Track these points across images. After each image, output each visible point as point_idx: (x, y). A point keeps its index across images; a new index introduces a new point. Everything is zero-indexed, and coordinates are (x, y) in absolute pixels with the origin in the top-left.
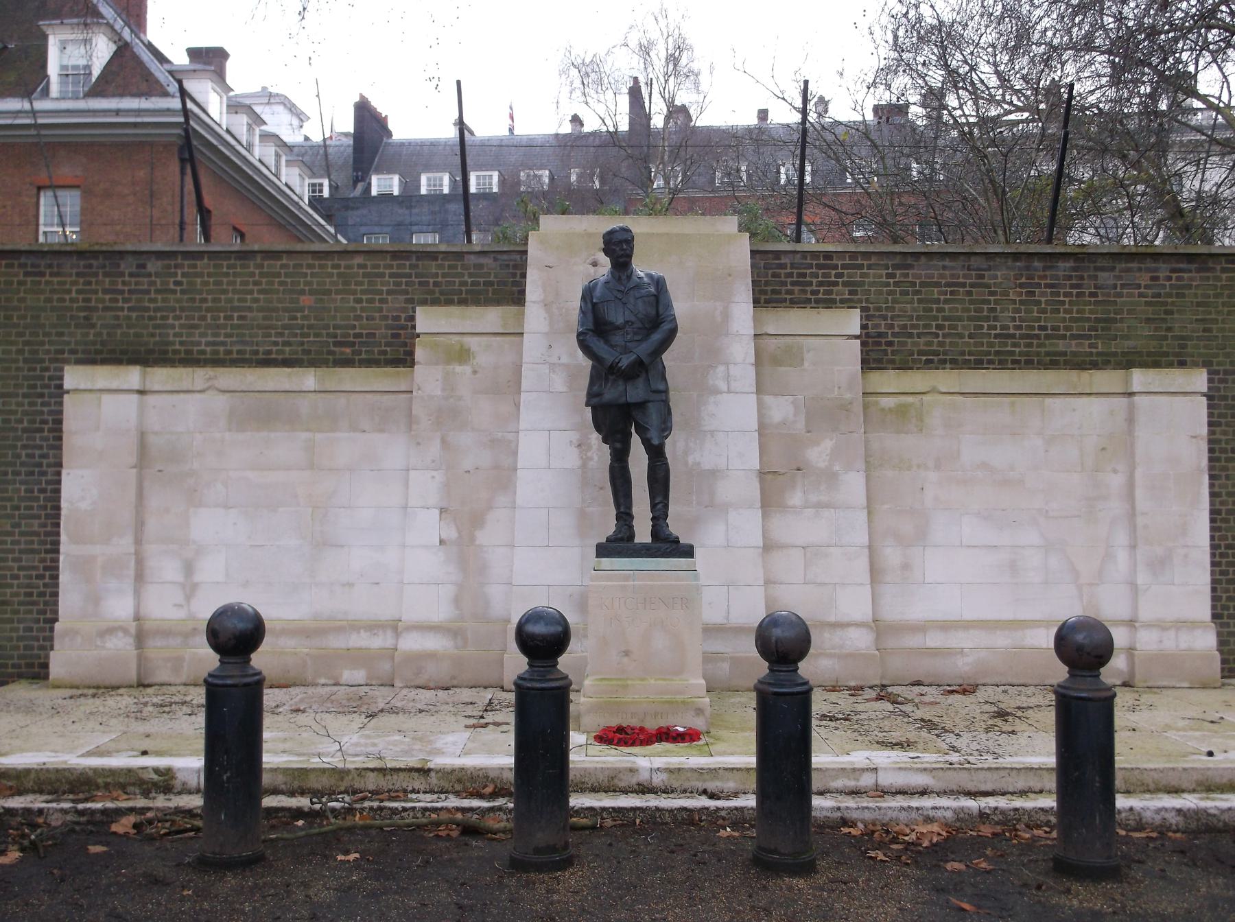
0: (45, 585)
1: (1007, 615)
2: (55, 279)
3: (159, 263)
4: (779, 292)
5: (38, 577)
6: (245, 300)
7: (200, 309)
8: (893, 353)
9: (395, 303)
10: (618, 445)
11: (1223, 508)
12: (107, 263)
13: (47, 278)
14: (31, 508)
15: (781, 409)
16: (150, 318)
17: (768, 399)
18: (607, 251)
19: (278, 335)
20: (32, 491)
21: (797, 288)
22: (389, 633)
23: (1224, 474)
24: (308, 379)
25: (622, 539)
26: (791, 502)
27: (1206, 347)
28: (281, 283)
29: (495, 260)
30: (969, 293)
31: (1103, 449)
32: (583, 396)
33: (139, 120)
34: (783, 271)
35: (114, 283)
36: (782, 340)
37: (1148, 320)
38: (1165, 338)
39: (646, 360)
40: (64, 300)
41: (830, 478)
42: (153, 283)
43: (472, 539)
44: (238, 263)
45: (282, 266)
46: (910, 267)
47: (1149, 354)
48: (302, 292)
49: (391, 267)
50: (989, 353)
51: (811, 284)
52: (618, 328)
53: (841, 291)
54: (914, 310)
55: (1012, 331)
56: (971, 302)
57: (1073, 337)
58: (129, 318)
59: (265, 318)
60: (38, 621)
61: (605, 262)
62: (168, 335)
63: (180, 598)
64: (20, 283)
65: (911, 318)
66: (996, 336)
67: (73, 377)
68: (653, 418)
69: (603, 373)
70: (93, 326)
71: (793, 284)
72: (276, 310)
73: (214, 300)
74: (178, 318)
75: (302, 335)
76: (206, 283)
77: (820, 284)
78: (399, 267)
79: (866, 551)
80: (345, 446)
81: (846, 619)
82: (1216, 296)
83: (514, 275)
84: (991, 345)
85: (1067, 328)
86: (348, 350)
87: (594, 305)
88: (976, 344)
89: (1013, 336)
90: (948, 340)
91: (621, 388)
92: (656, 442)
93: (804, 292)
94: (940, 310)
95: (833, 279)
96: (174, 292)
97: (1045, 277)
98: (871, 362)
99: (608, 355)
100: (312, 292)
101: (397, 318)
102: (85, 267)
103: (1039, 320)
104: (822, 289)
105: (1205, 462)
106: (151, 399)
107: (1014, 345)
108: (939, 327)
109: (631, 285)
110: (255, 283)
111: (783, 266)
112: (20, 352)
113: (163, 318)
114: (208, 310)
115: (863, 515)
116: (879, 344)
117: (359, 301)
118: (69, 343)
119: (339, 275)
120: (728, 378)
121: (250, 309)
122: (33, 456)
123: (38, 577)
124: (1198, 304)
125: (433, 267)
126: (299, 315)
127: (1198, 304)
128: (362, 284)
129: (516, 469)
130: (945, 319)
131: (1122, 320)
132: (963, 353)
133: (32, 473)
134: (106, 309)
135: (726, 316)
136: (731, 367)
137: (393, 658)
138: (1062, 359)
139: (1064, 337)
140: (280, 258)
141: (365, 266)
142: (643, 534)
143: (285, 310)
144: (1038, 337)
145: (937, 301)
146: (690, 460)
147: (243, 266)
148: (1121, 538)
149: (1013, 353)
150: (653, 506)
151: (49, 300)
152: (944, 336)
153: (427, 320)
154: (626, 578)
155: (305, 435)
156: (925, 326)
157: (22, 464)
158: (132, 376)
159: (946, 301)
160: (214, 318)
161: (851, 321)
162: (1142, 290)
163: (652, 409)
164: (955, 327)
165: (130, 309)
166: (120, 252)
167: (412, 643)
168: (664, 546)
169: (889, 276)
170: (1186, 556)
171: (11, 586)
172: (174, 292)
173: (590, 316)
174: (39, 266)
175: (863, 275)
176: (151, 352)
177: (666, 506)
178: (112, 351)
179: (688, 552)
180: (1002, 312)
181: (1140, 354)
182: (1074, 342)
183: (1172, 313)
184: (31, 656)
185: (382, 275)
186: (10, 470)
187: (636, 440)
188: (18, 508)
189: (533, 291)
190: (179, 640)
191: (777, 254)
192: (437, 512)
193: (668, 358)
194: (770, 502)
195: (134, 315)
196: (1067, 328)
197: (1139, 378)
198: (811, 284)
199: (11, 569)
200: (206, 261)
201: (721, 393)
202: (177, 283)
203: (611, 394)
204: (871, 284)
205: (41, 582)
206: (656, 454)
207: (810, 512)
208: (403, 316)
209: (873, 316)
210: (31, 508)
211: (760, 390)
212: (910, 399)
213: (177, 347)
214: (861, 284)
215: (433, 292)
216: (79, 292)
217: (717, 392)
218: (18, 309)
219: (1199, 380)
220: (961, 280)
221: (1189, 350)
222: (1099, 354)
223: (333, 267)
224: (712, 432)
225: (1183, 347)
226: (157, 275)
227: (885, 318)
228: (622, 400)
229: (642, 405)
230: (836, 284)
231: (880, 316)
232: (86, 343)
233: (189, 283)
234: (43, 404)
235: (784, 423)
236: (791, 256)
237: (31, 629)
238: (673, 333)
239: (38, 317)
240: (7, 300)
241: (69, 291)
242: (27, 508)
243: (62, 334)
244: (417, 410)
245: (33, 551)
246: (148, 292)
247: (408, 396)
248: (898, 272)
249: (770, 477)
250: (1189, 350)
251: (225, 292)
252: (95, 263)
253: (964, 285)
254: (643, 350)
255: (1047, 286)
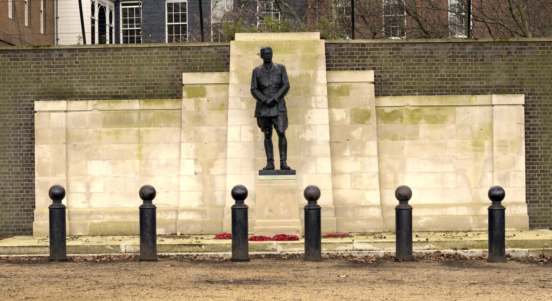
0: (24, 195)
1: (439, 201)
2: (24, 62)
3: (69, 54)
4: (342, 61)
5: (20, 192)
6: (106, 69)
7: (86, 74)
8: (393, 88)
9: (171, 70)
10: (267, 133)
11: (540, 154)
12: (46, 54)
13: (20, 61)
14: (17, 162)
15: (340, 114)
16: (65, 78)
17: (334, 110)
18: (262, 56)
19: (120, 84)
20: (17, 155)
21: (349, 60)
22: (174, 213)
23: (540, 139)
24: (136, 104)
25: (269, 169)
26: (345, 154)
27: (532, 83)
28: (121, 62)
29: (215, 49)
30: (426, 61)
31: (481, 129)
32: (253, 114)
33: (113, 34)
34: (343, 52)
35: (49, 63)
36: (340, 84)
37: (506, 71)
38: (514, 79)
39: (277, 100)
40: (28, 71)
41: (363, 145)
42: (66, 63)
43: (209, 172)
44: (103, 53)
45: (122, 54)
46: (399, 49)
47: (507, 86)
48: (131, 65)
49: (170, 53)
50: (435, 87)
51: (356, 57)
52: (266, 88)
53: (369, 61)
54: (402, 68)
55: (445, 77)
56: (427, 64)
57: (473, 80)
58: (56, 78)
59: (115, 77)
60: (21, 211)
61: (262, 61)
62: (73, 85)
63: (85, 199)
64: (9, 64)
65: (401, 72)
66: (439, 79)
67: (38, 105)
68: (281, 123)
69: (261, 105)
70: (41, 82)
71: (348, 57)
72: (120, 73)
73: (93, 70)
74: (77, 78)
75: (132, 84)
76: (89, 62)
77: (360, 57)
78: (173, 53)
79: (377, 175)
80: (153, 133)
81: (368, 204)
82: (536, 60)
83: (224, 56)
84: (436, 83)
85: (471, 76)
86: (152, 91)
87: (257, 78)
88: (430, 83)
89: (446, 79)
90: (417, 82)
91: (268, 111)
92: (281, 132)
93: (353, 61)
94: (413, 68)
95: (366, 55)
96: (75, 66)
97: (460, 53)
98: (378, 93)
99: (263, 98)
100: (135, 65)
101: (172, 76)
102: (36, 56)
103: (458, 72)
104: (361, 60)
105: (523, 135)
106: (69, 114)
107: (447, 83)
108: (413, 76)
109: (271, 70)
110: (110, 62)
111: (343, 50)
112: (9, 94)
113: (71, 78)
114: (90, 74)
115: (375, 160)
116: (386, 84)
117: (156, 69)
118: (31, 90)
119: (147, 57)
120: (316, 102)
121: (108, 73)
122: (17, 139)
123: (20, 192)
124: (529, 64)
125: (188, 53)
126: (130, 75)
127: (529, 64)
128: (157, 61)
129: (226, 142)
130: (416, 72)
131: (494, 72)
132: (424, 87)
133: (16, 147)
134: (46, 74)
135: (315, 76)
136: (317, 97)
137: (176, 224)
138: (468, 89)
139: (469, 80)
140: (121, 51)
141: (158, 53)
142: (277, 166)
143: (124, 73)
144: (457, 80)
145: (412, 64)
146: (301, 137)
147: (105, 55)
148: (489, 168)
149: (446, 87)
150: (281, 156)
151: (21, 71)
152: (415, 80)
153: (188, 78)
154: (270, 183)
155: (136, 129)
156: (407, 76)
157: (12, 143)
158: (62, 104)
159: (416, 64)
160: (93, 78)
161: (370, 75)
162: (504, 58)
163: (280, 118)
164: (420, 76)
165: (57, 74)
166: (52, 49)
167: (183, 216)
168: (284, 171)
169: (390, 53)
170: (515, 175)
171: (9, 196)
172: (75, 66)
173: (256, 82)
174: (17, 56)
175: (379, 53)
176: (66, 93)
177: (286, 156)
178: (50, 93)
179: (294, 173)
180: (441, 68)
181: (502, 86)
182: (473, 82)
183: (517, 68)
184: (19, 226)
185: (166, 57)
186: (7, 145)
187: (274, 131)
188: (11, 162)
189: (232, 67)
190: (85, 217)
191: (341, 45)
192: (193, 161)
193: (285, 98)
194: (334, 155)
195: (58, 77)
196: (471, 76)
197: (496, 99)
198: (356, 57)
199: (9, 188)
200: (89, 52)
201: (313, 108)
202: (76, 62)
203: (264, 113)
204: (383, 57)
205: (22, 194)
206: (282, 136)
207: (352, 158)
208: (175, 75)
209: (384, 71)
210: (17, 162)
211: (330, 106)
212: (397, 109)
213: (77, 91)
214: (378, 57)
215: (188, 64)
216: (34, 67)
217: (311, 107)
218: (8, 75)
219: (521, 99)
220: (423, 55)
221: (525, 84)
222: (484, 87)
223: (144, 54)
224: (309, 125)
225: (521, 83)
226: (68, 59)
227: (389, 72)
228: (269, 115)
229: (276, 117)
230: (367, 57)
231: (386, 71)
232: (38, 90)
233: (82, 62)
234: (20, 117)
235: (342, 120)
236: (347, 45)
237: (18, 214)
238: (288, 89)
239: (17, 79)
240: (3, 71)
241: (30, 67)
242: (15, 162)
243: (28, 86)
244: (184, 118)
245: (18, 181)
246: (64, 66)
247: (180, 111)
248: (395, 52)
249: (334, 144)
250: (525, 84)
251: (97, 66)
252: (41, 54)
253: (424, 57)
254: (276, 97)
255: (461, 57)
